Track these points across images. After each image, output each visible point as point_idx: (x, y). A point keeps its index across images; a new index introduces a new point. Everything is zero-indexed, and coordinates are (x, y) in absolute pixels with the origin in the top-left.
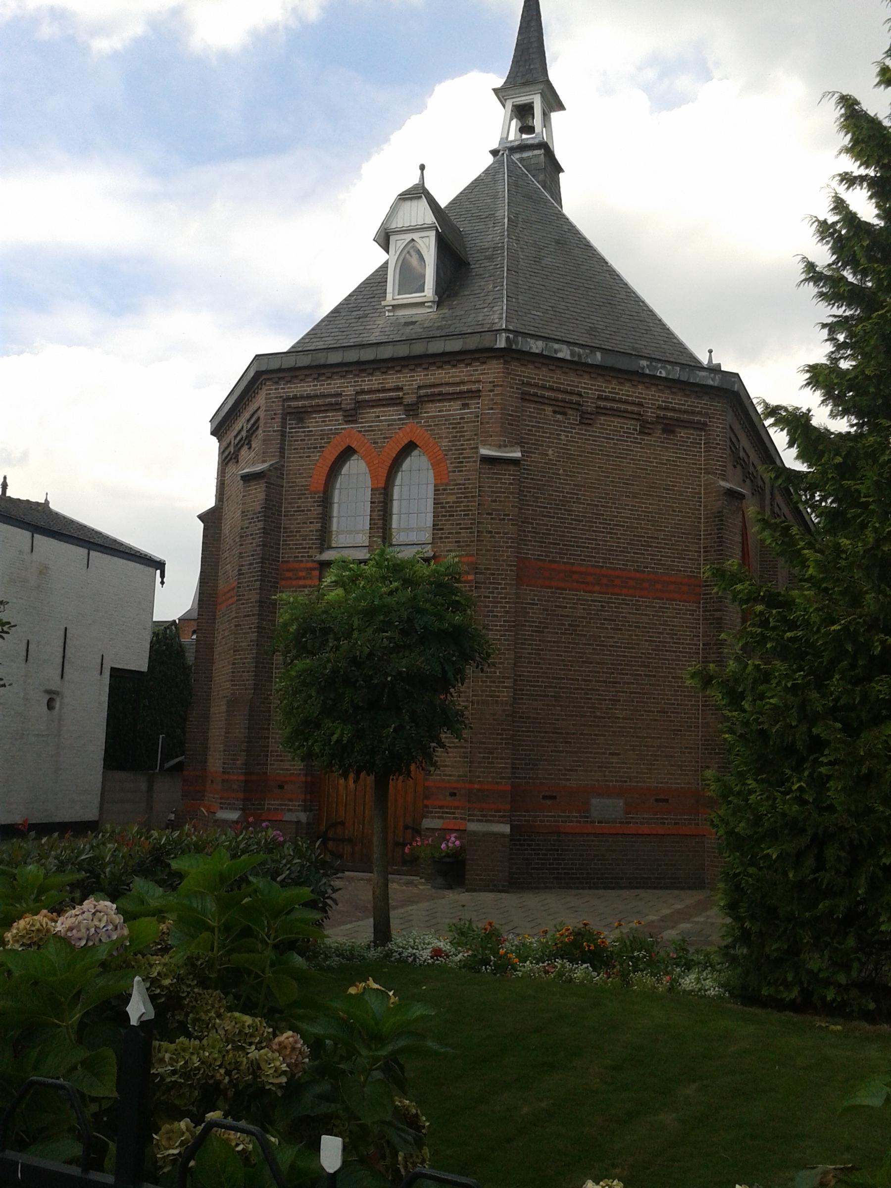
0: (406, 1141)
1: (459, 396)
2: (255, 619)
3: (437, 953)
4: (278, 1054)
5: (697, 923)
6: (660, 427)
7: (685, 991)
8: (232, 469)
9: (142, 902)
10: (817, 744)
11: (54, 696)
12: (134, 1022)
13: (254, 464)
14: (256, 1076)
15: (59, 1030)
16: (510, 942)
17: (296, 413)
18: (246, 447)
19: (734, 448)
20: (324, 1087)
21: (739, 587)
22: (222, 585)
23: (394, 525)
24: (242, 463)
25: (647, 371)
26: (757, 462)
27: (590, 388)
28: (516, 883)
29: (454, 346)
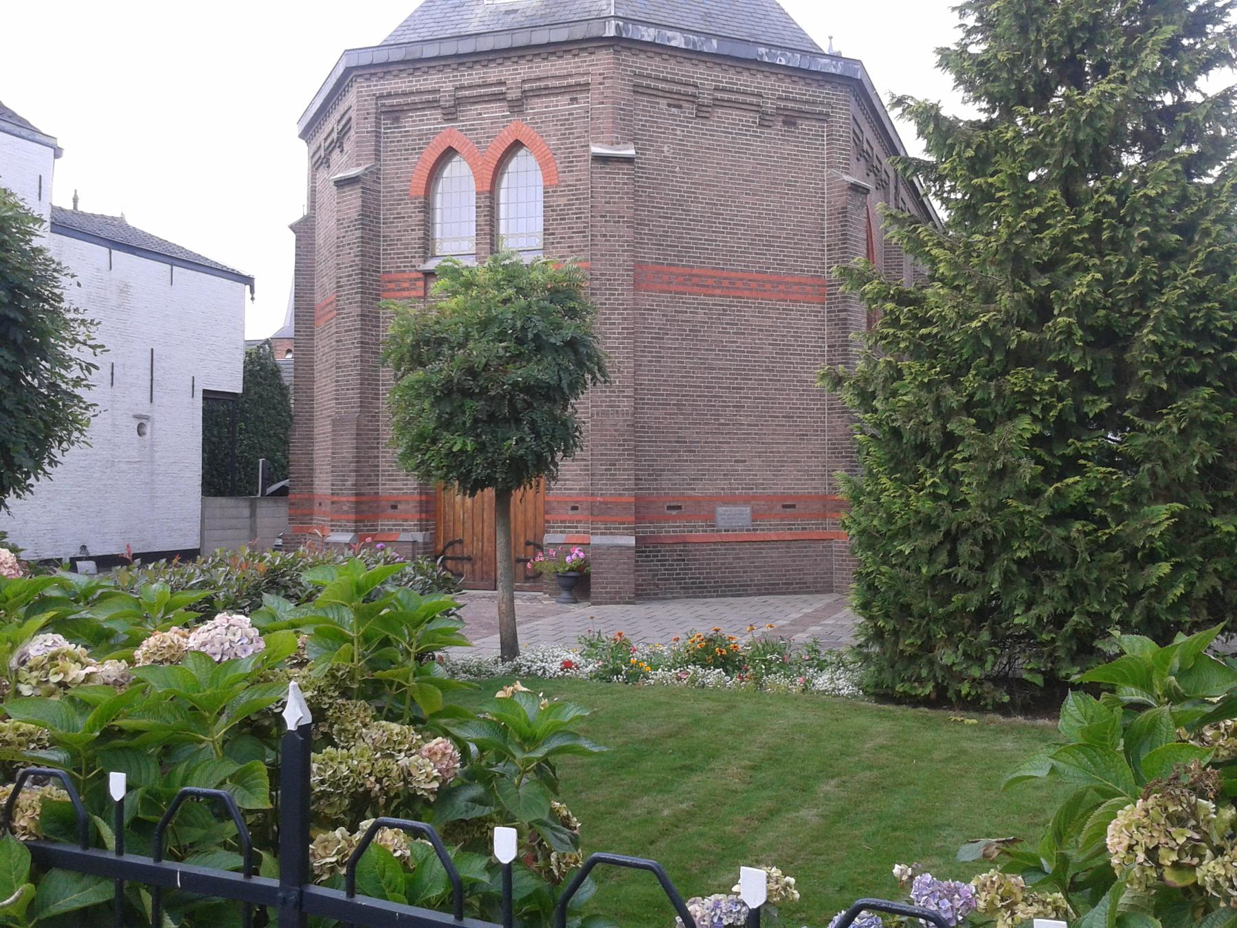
0: (561, 840)
1: (567, 89)
2: (357, 334)
3: (567, 665)
4: (428, 761)
5: (826, 625)
6: (781, 118)
7: (818, 691)
8: (323, 174)
9: (274, 618)
10: (950, 441)
11: (144, 421)
12: (291, 726)
13: (347, 167)
14: (406, 782)
15: (203, 745)
16: (640, 653)
17: (391, 112)
18: (337, 150)
19: (858, 141)
20: (477, 790)
21: (867, 287)
22: (318, 299)
23: (502, 230)
24: (333, 168)
25: (766, 59)
26: (882, 156)
27: (705, 78)
28: (641, 594)
29: (561, 35)
